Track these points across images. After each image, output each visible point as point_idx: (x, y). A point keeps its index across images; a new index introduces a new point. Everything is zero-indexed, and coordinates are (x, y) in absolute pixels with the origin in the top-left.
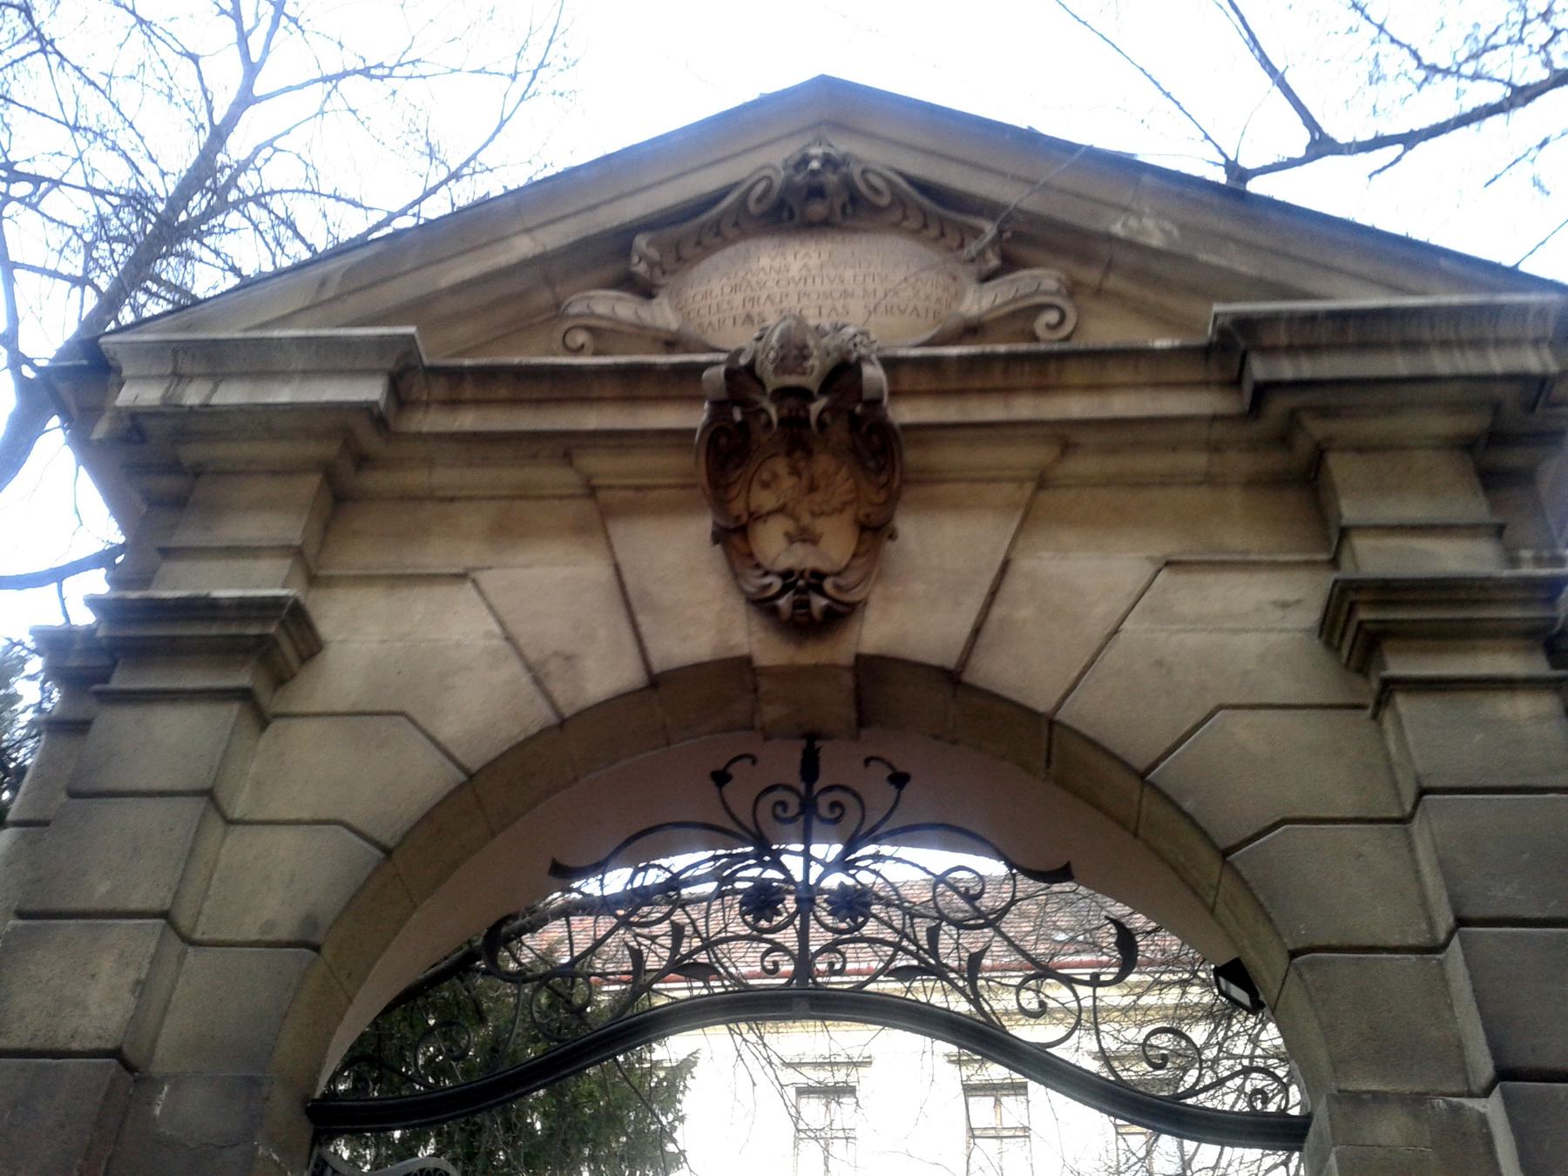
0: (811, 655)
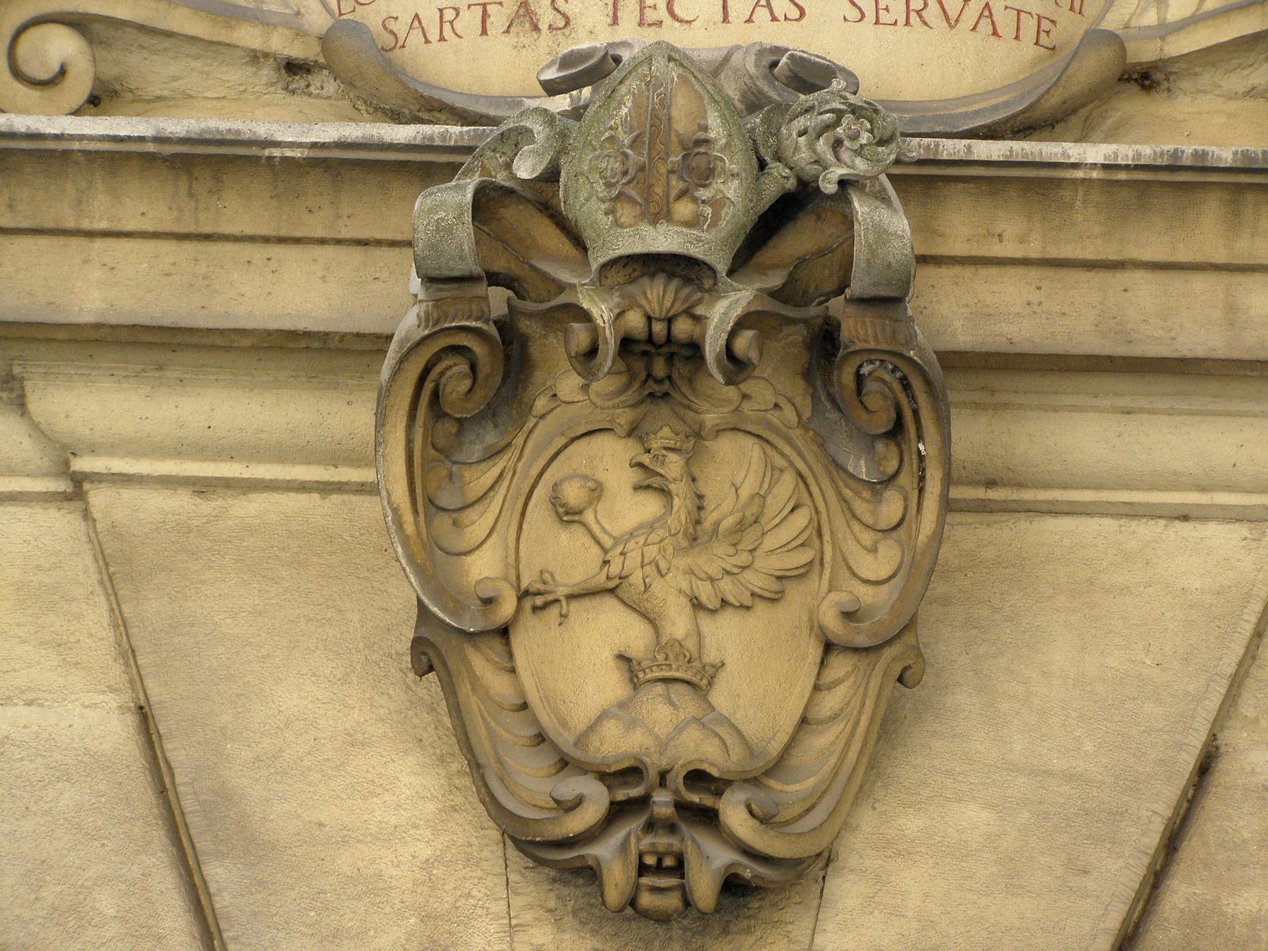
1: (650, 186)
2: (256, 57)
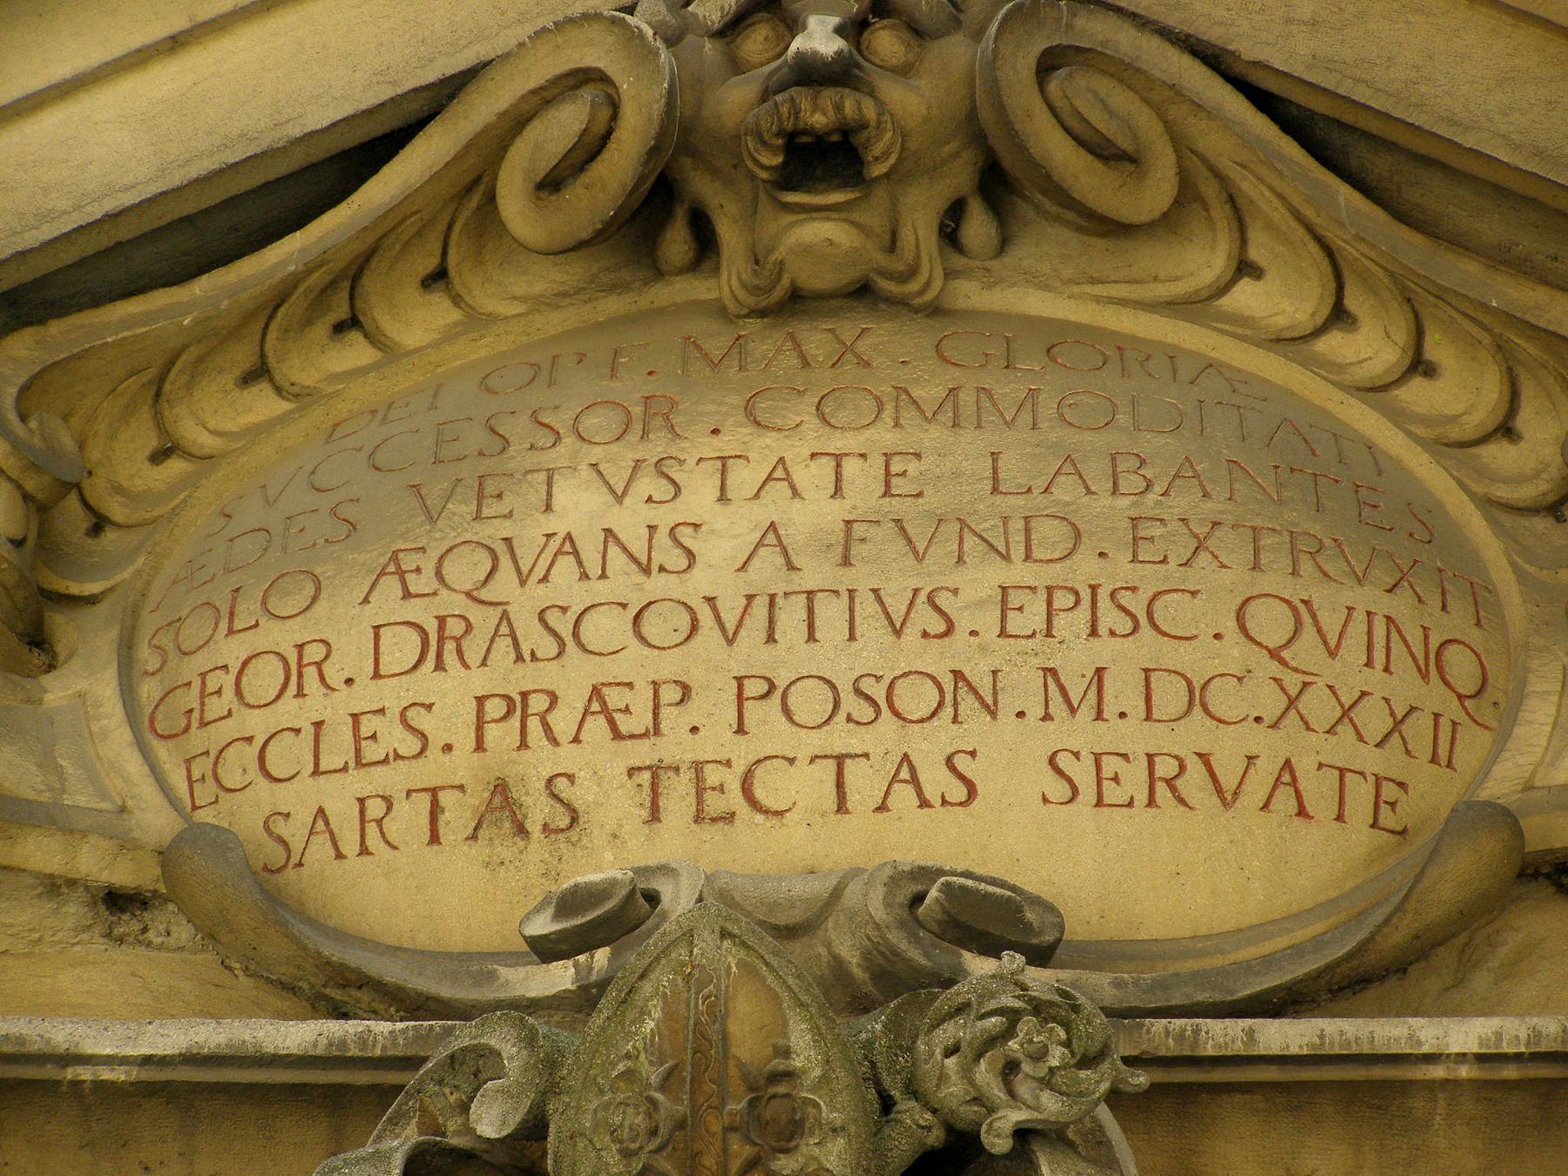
1: (696, 1156)
2: (54, 886)
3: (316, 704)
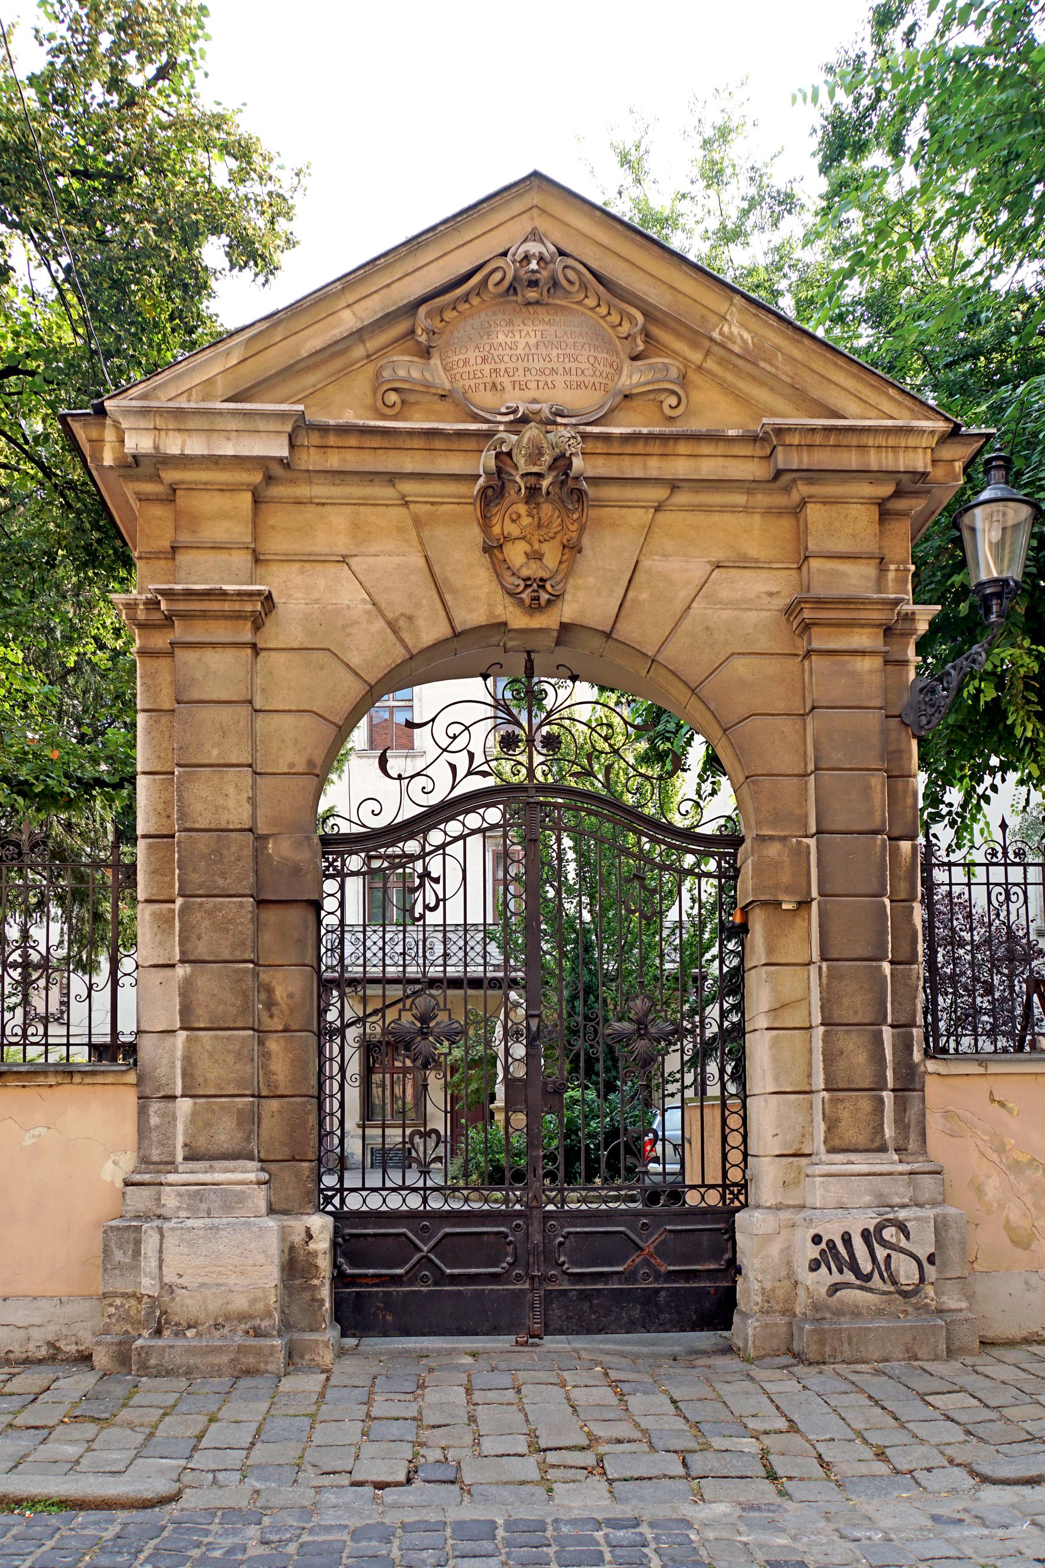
0: (537, 622)
3: (468, 369)
